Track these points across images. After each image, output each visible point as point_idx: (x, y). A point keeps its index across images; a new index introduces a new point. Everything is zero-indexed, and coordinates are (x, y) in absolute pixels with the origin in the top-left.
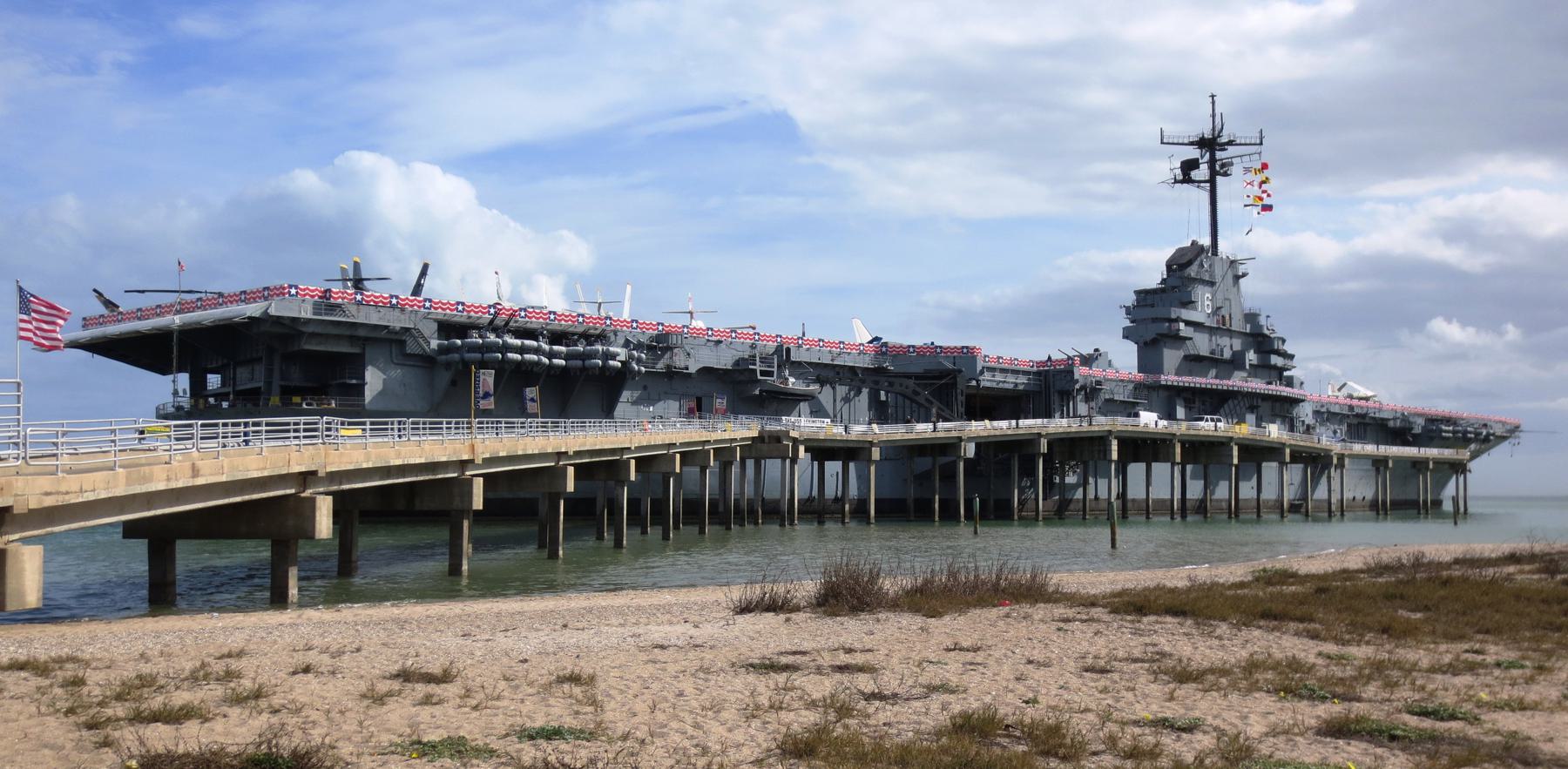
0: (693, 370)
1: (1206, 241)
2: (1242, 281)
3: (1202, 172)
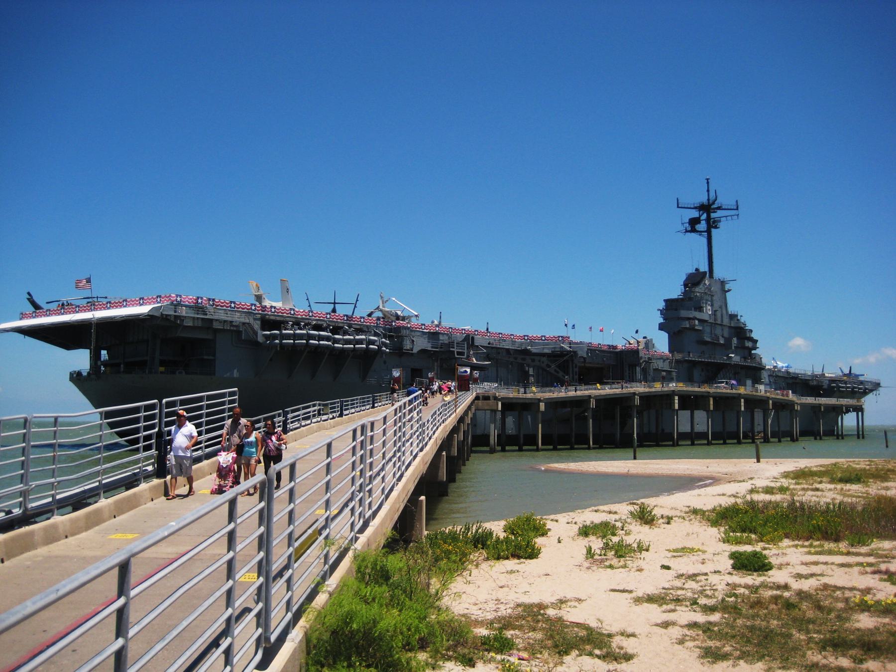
0: (415, 351)
1: (704, 268)
2: (727, 294)
3: (702, 226)
